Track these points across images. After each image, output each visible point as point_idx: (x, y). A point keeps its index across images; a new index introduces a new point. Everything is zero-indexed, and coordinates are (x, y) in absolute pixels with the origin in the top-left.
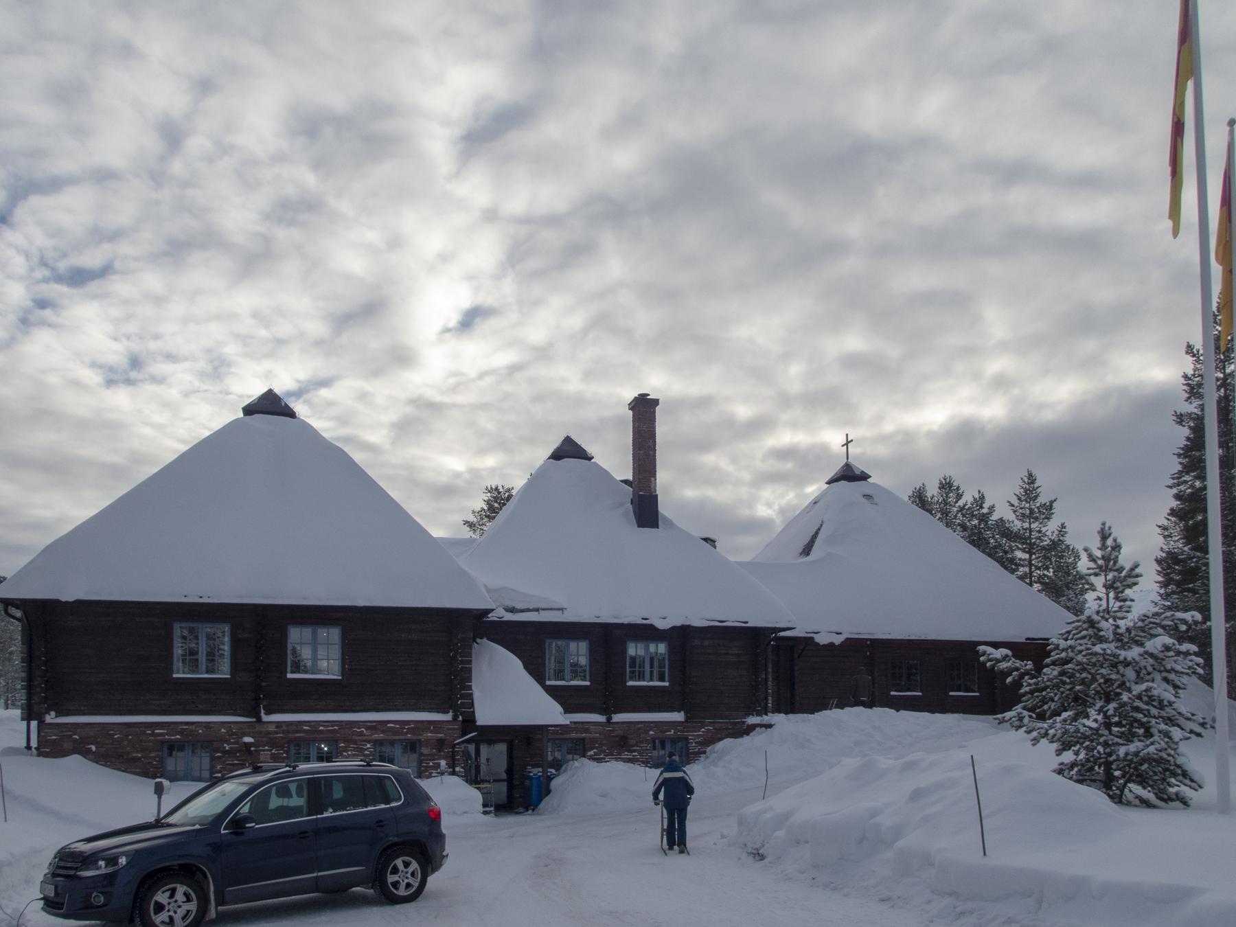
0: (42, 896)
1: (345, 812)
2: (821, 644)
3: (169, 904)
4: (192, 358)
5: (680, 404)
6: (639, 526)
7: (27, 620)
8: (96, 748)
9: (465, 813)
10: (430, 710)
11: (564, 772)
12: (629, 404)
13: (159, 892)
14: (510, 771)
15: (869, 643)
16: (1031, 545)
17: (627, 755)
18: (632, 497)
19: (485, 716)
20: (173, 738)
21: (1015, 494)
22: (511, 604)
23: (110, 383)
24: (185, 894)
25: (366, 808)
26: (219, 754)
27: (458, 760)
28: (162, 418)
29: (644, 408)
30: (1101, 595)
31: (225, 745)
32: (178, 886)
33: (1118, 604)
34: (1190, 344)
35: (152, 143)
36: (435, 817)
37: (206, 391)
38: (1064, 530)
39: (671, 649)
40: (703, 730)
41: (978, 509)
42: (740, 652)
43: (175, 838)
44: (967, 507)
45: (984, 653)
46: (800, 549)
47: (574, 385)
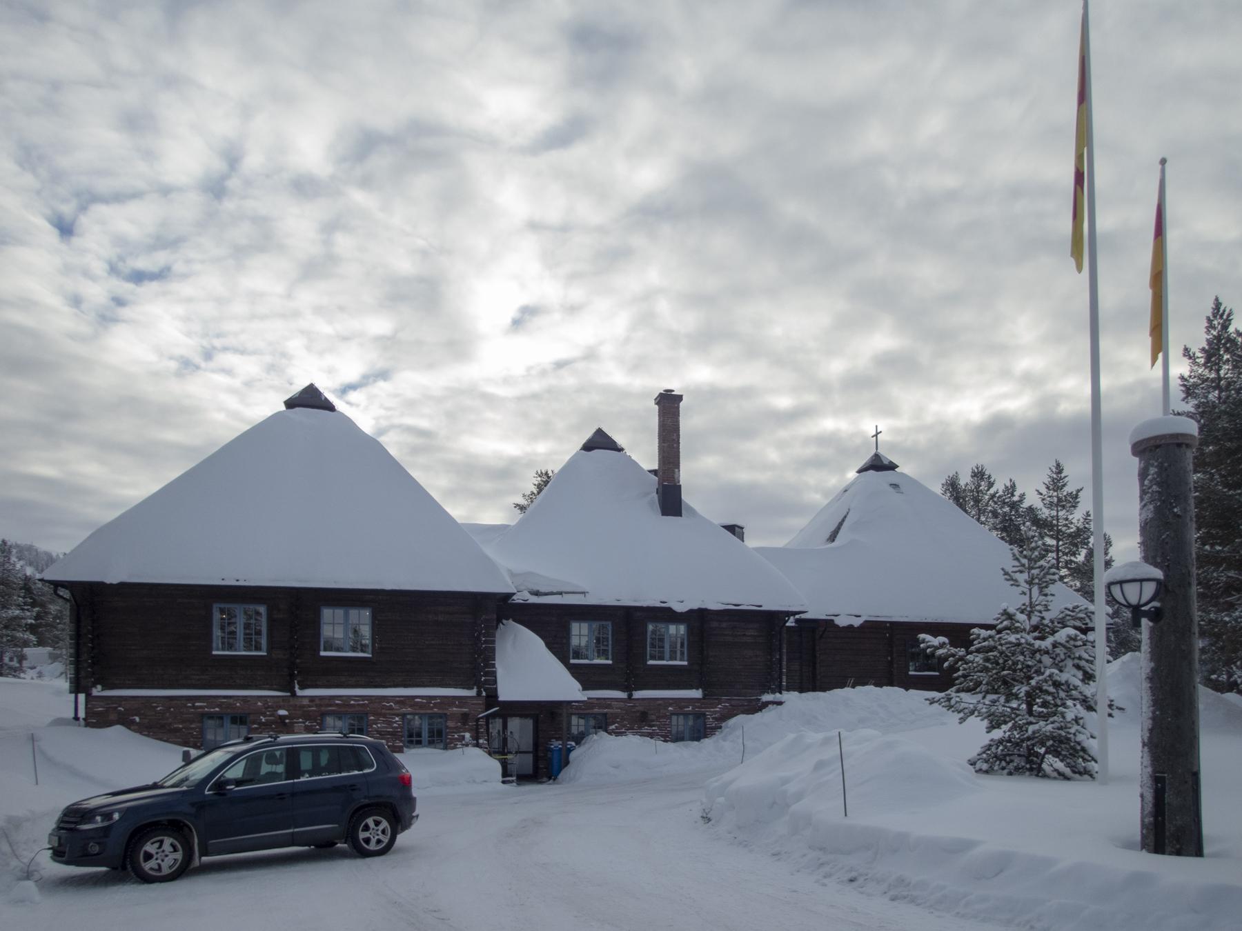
0: (50, 846)
1: (320, 777)
3: (157, 853)
5: (713, 394)
6: (663, 515)
7: (75, 602)
8: (140, 719)
9: (485, 781)
10: (455, 686)
11: (584, 744)
12: (655, 399)
13: (149, 843)
14: (536, 744)
15: (888, 625)
16: (1059, 531)
17: (647, 729)
18: (657, 487)
19: (507, 692)
20: (212, 710)
21: (1044, 483)
22: (536, 588)
24: (172, 845)
25: (340, 773)
26: (256, 726)
27: (482, 732)
28: (232, 403)
29: (669, 403)
30: (1025, 590)
31: (262, 717)
32: (166, 838)
33: (1042, 598)
34: (1187, 346)
36: (406, 782)
38: (1089, 518)
39: (690, 631)
40: (720, 706)
41: (1010, 497)
42: (756, 634)
43: (165, 798)
44: (997, 495)
45: (923, 641)
46: (828, 535)
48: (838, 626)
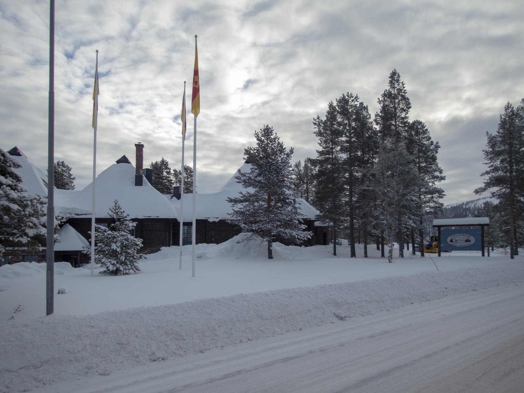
2: (210, 222)
4: (142, 104)
23: (111, 114)
28: (131, 126)
35: (127, 26)
37: (147, 116)
47: (289, 108)
48: (209, 222)
